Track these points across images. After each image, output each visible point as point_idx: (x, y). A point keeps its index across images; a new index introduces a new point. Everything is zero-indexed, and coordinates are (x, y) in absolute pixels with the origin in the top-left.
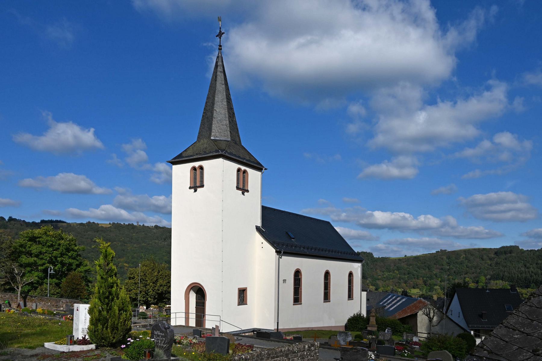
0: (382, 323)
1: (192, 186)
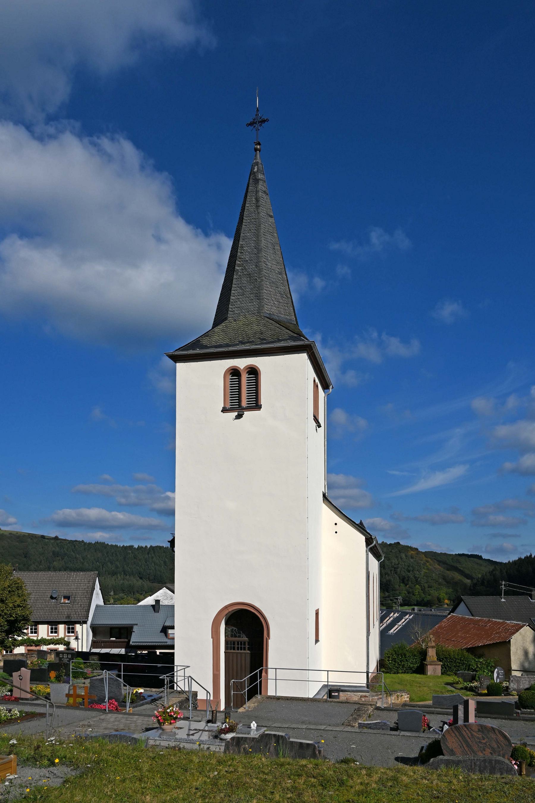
0: (446, 658)
1: (228, 406)
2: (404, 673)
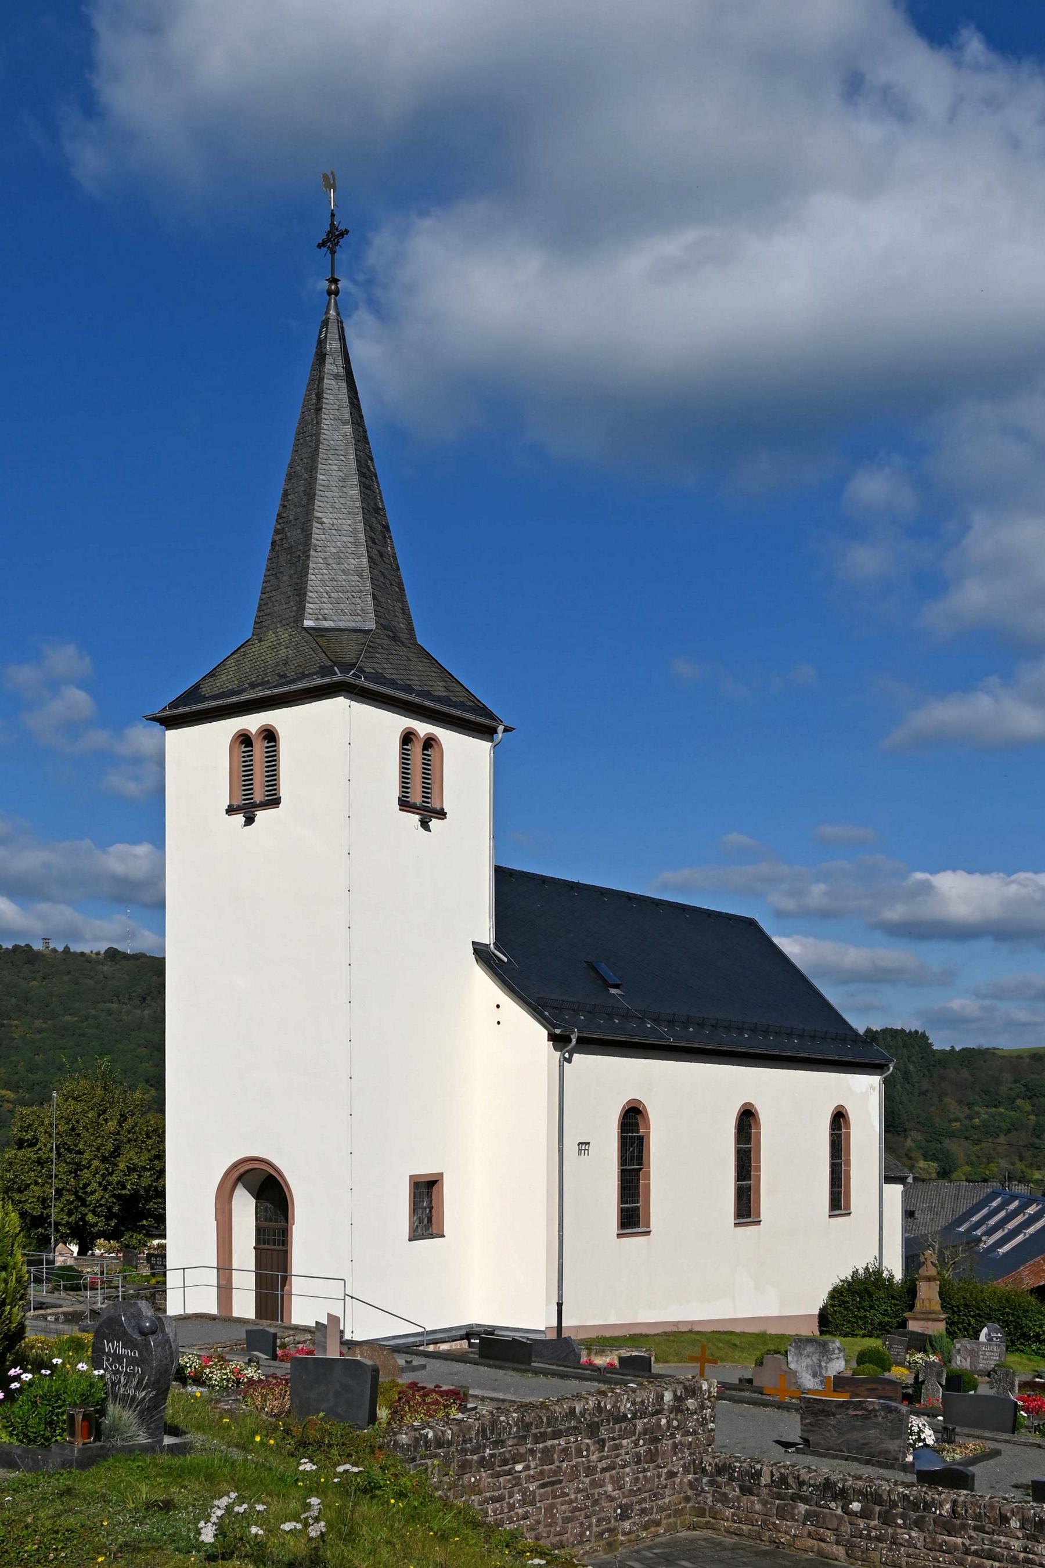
1: (235, 803)
2: (870, 1336)
